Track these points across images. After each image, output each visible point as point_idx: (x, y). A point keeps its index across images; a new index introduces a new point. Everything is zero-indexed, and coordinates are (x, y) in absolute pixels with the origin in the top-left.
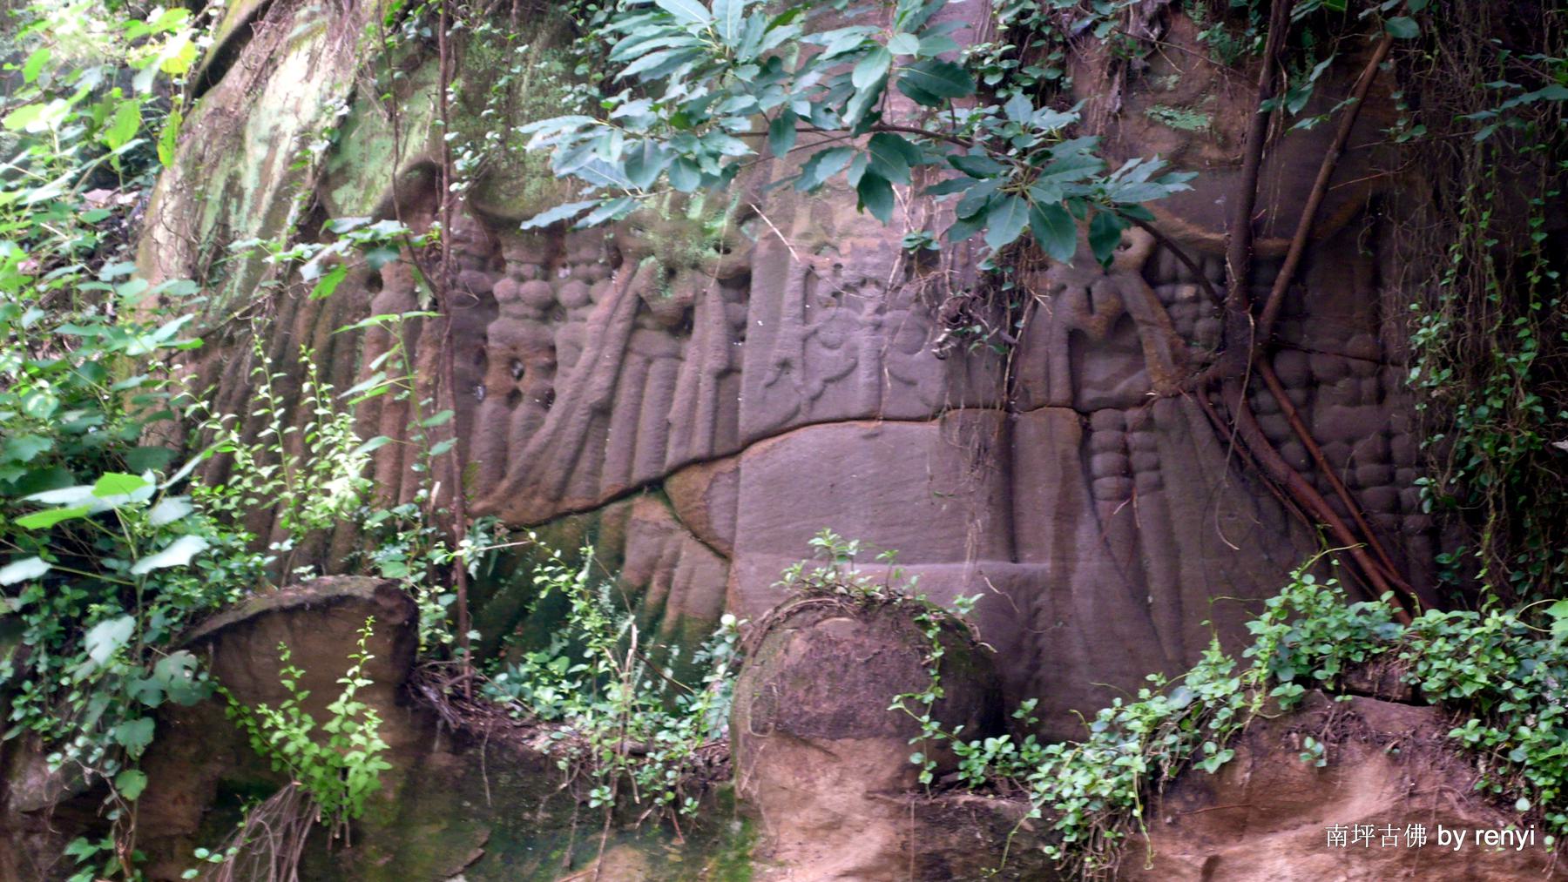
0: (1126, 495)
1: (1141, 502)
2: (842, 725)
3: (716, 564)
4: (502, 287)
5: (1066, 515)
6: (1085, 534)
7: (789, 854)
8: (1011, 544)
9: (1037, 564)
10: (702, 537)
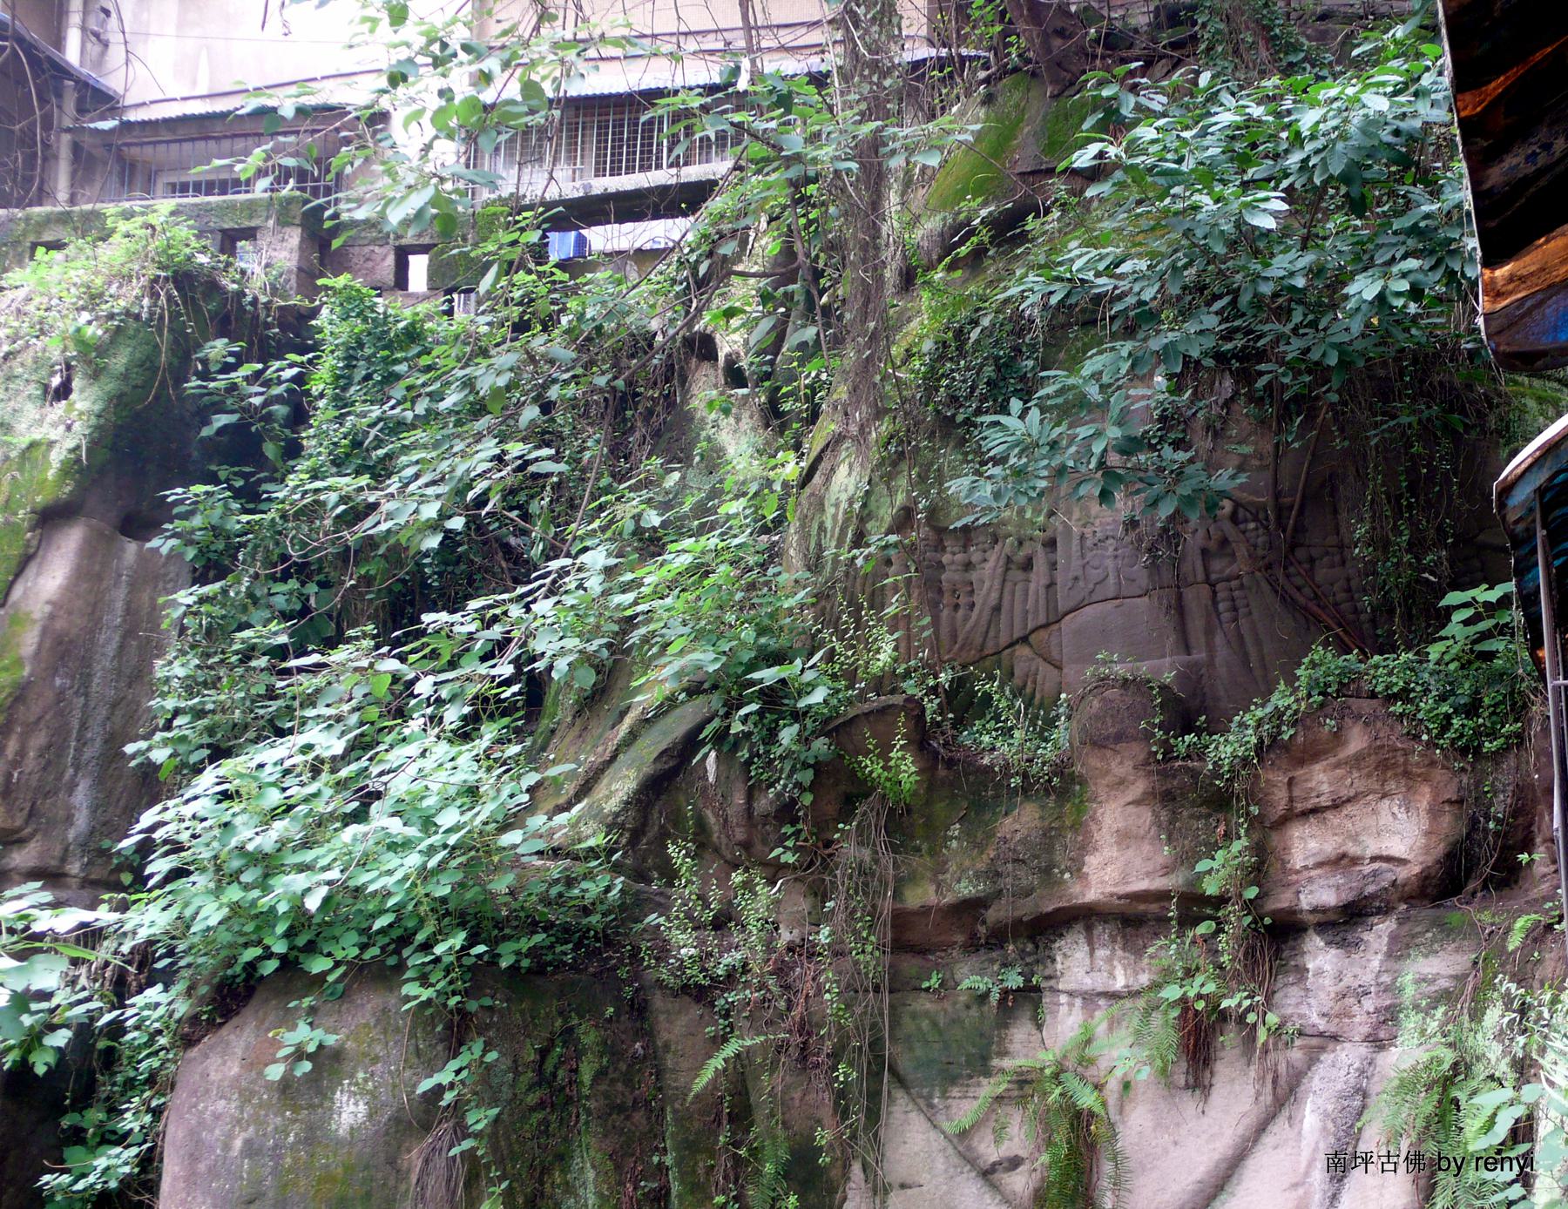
0: (1235, 619)
1: (1242, 621)
2: (1119, 737)
4: (946, 559)
5: (1209, 632)
6: (1219, 639)
7: (1102, 794)
9: (1199, 655)
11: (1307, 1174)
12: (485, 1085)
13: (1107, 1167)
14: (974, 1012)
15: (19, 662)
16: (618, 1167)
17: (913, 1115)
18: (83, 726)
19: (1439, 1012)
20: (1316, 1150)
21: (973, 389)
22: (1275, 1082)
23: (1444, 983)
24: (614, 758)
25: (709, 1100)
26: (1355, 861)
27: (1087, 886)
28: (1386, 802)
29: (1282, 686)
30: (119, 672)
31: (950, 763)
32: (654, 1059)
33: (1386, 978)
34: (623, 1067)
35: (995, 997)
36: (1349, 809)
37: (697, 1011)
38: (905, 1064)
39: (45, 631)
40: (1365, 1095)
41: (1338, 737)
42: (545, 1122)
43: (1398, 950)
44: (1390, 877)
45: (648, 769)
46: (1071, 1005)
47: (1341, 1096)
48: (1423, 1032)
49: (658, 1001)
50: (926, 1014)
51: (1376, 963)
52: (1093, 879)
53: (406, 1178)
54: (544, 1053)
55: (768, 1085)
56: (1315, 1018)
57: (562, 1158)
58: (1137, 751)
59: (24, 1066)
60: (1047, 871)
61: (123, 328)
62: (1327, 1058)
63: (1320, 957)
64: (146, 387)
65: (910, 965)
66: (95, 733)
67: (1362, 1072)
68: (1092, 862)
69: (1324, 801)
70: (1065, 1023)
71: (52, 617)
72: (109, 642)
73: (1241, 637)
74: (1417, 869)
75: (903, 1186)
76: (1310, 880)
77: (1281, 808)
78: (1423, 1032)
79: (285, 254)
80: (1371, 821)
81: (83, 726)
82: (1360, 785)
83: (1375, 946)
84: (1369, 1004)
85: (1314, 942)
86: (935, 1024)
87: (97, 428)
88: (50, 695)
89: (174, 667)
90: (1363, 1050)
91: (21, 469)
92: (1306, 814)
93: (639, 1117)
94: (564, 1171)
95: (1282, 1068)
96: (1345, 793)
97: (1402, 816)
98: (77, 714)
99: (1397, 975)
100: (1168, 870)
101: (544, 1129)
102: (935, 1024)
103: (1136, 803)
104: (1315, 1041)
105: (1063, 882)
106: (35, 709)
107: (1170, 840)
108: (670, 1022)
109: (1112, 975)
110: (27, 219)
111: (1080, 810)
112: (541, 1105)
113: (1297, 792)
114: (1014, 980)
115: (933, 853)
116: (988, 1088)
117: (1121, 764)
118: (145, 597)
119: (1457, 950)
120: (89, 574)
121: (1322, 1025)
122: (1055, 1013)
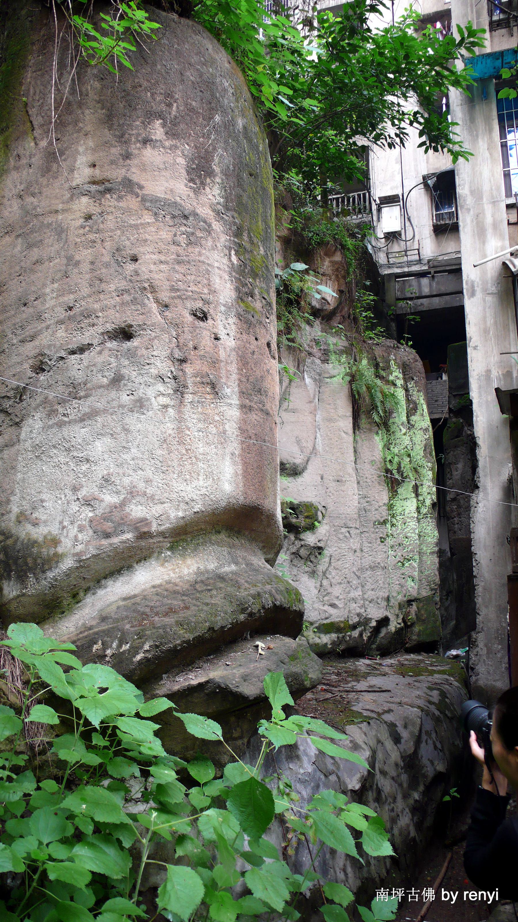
19: (344, 356)
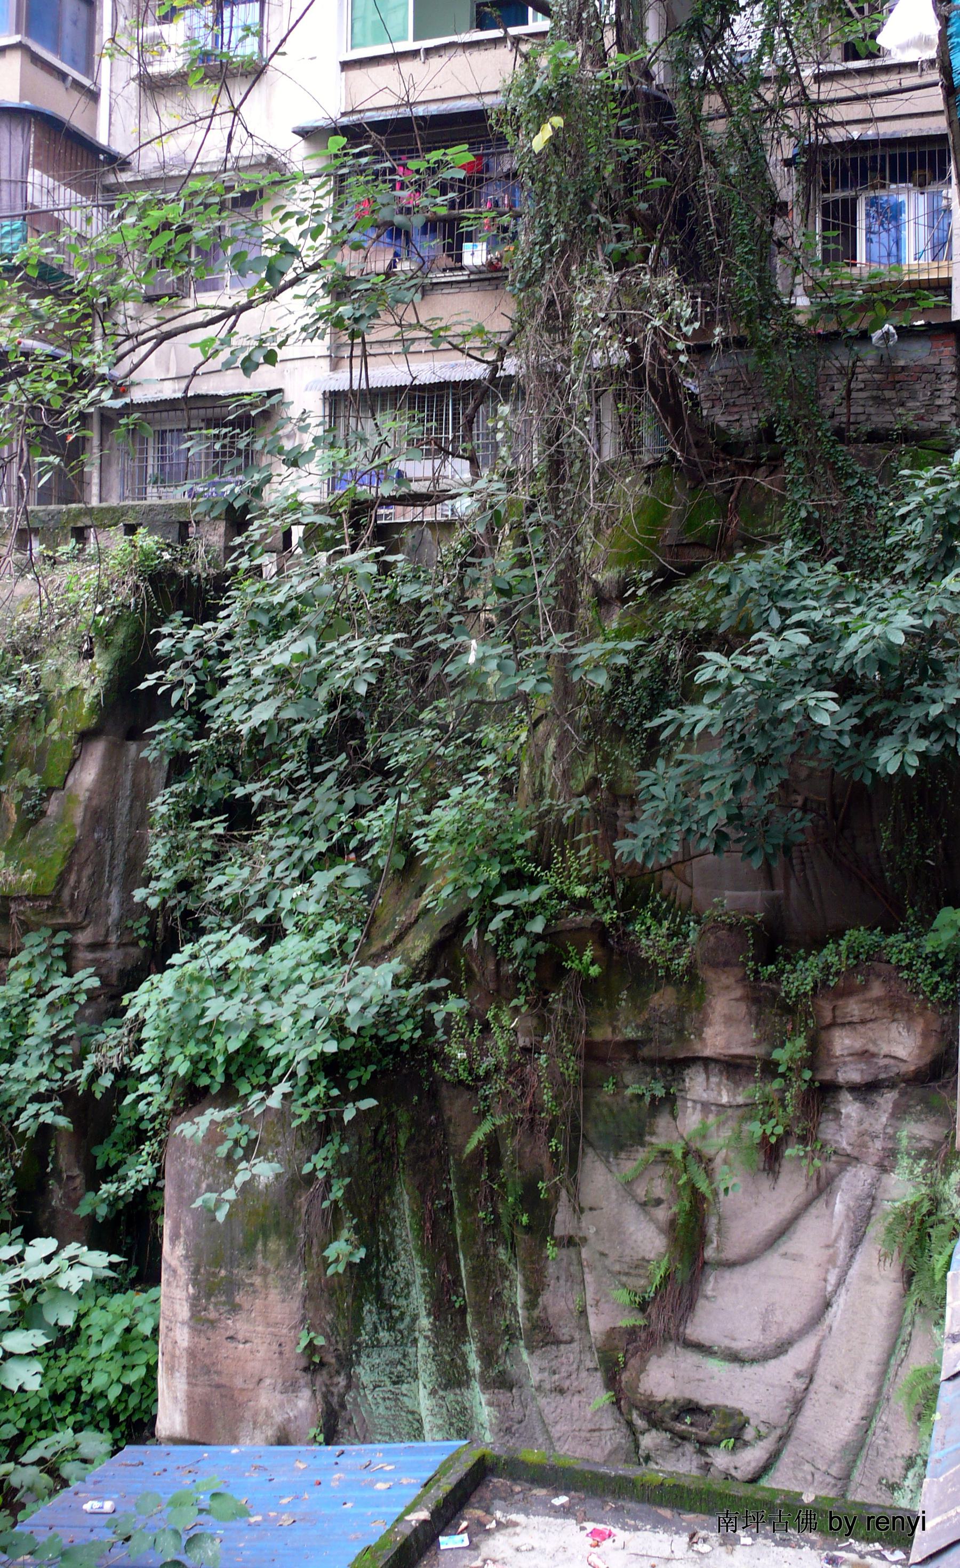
0: (803, 870)
1: (808, 872)
2: (726, 964)
3: (688, 889)
4: (620, 812)
5: (786, 879)
6: (793, 882)
7: (715, 992)
8: (772, 885)
9: (779, 892)
10: (685, 883)
11: (836, 1240)
12: (341, 1164)
13: (714, 1220)
14: (635, 1105)
15: (73, 827)
16: (422, 1193)
17: (598, 1164)
18: (112, 858)
19: (923, 1162)
20: (842, 1227)
21: (636, 709)
22: (818, 1179)
23: (926, 1144)
24: (416, 921)
25: (477, 1153)
26: (873, 1055)
27: (705, 1046)
28: (895, 1025)
29: (831, 946)
30: (131, 822)
31: (622, 953)
32: (442, 1125)
33: (890, 1130)
34: (424, 1132)
35: (647, 1099)
36: (870, 1025)
37: (467, 1096)
38: (592, 1135)
39: (86, 808)
40: (874, 1199)
41: (865, 987)
42: (380, 1170)
43: (900, 1112)
44: (896, 1070)
45: (436, 936)
46: (694, 1108)
47: (858, 1198)
48: (911, 1172)
49: (444, 1092)
50: (606, 1104)
51: (884, 1119)
52: (709, 1042)
53: (299, 1212)
54: (376, 1132)
55: (510, 1145)
56: (844, 1145)
57: (390, 1189)
58: (738, 972)
59: (89, 1093)
60: (680, 1032)
61: (121, 615)
62: (851, 1170)
63: (850, 1108)
64: (136, 649)
65: (597, 1071)
66: (120, 861)
67: (872, 1185)
68: (708, 1032)
69: (855, 1019)
70: (691, 1120)
71: (90, 799)
72: (123, 806)
73: (807, 884)
74: (913, 1068)
75: (591, 1209)
76: (845, 1063)
77: (828, 1020)
78: (911, 1172)
79: (216, 538)
80: (885, 1034)
81: (112, 858)
82: (878, 1013)
83: (884, 1107)
84: (878, 1144)
85: (846, 1096)
86: (611, 1111)
87: (109, 681)
88: (92, 844)
89: (158, 849)
90: (874, 1171)
91: (67, 703)
92: (843, 1025)
93: (434, 1161)
94: (391, 1196)
95: (823, 1172)
96: (868, 1017)
97: (904, 1033)
98: (108, 851)
99: (897, 1129)
100: (757, 1043)
101: (379, 1172)
102: (611, 1111)
103: (737, 1000)
104: (844, 1159)
105: (690, 1040)
106: (84, 855)
107: (757, 1026)
108: (451, 1104)
109: (720, 1094)
110: (69, 511)
111: (701, 998)
112: (376, 1161)
113: (838, 1013)
114: (660, 1092)
115: (611, 1007)
116: (642, 1154)
117: (727, 979)
118: (143, 775)
119: (936, 1122)
120: (110, 770)
121: (849, 1149)
122: (684, 1112)
